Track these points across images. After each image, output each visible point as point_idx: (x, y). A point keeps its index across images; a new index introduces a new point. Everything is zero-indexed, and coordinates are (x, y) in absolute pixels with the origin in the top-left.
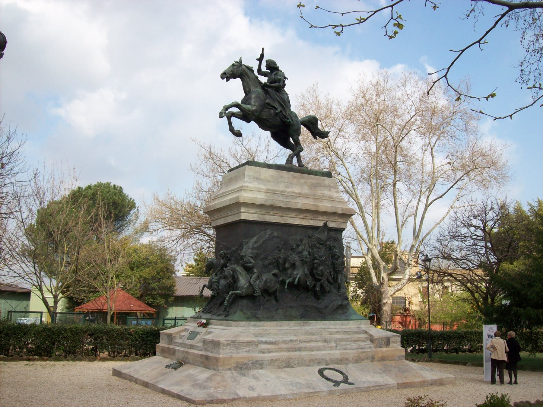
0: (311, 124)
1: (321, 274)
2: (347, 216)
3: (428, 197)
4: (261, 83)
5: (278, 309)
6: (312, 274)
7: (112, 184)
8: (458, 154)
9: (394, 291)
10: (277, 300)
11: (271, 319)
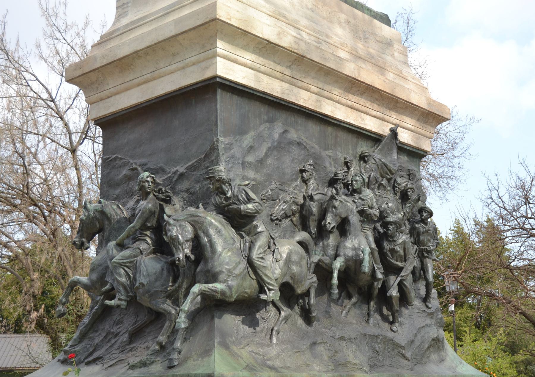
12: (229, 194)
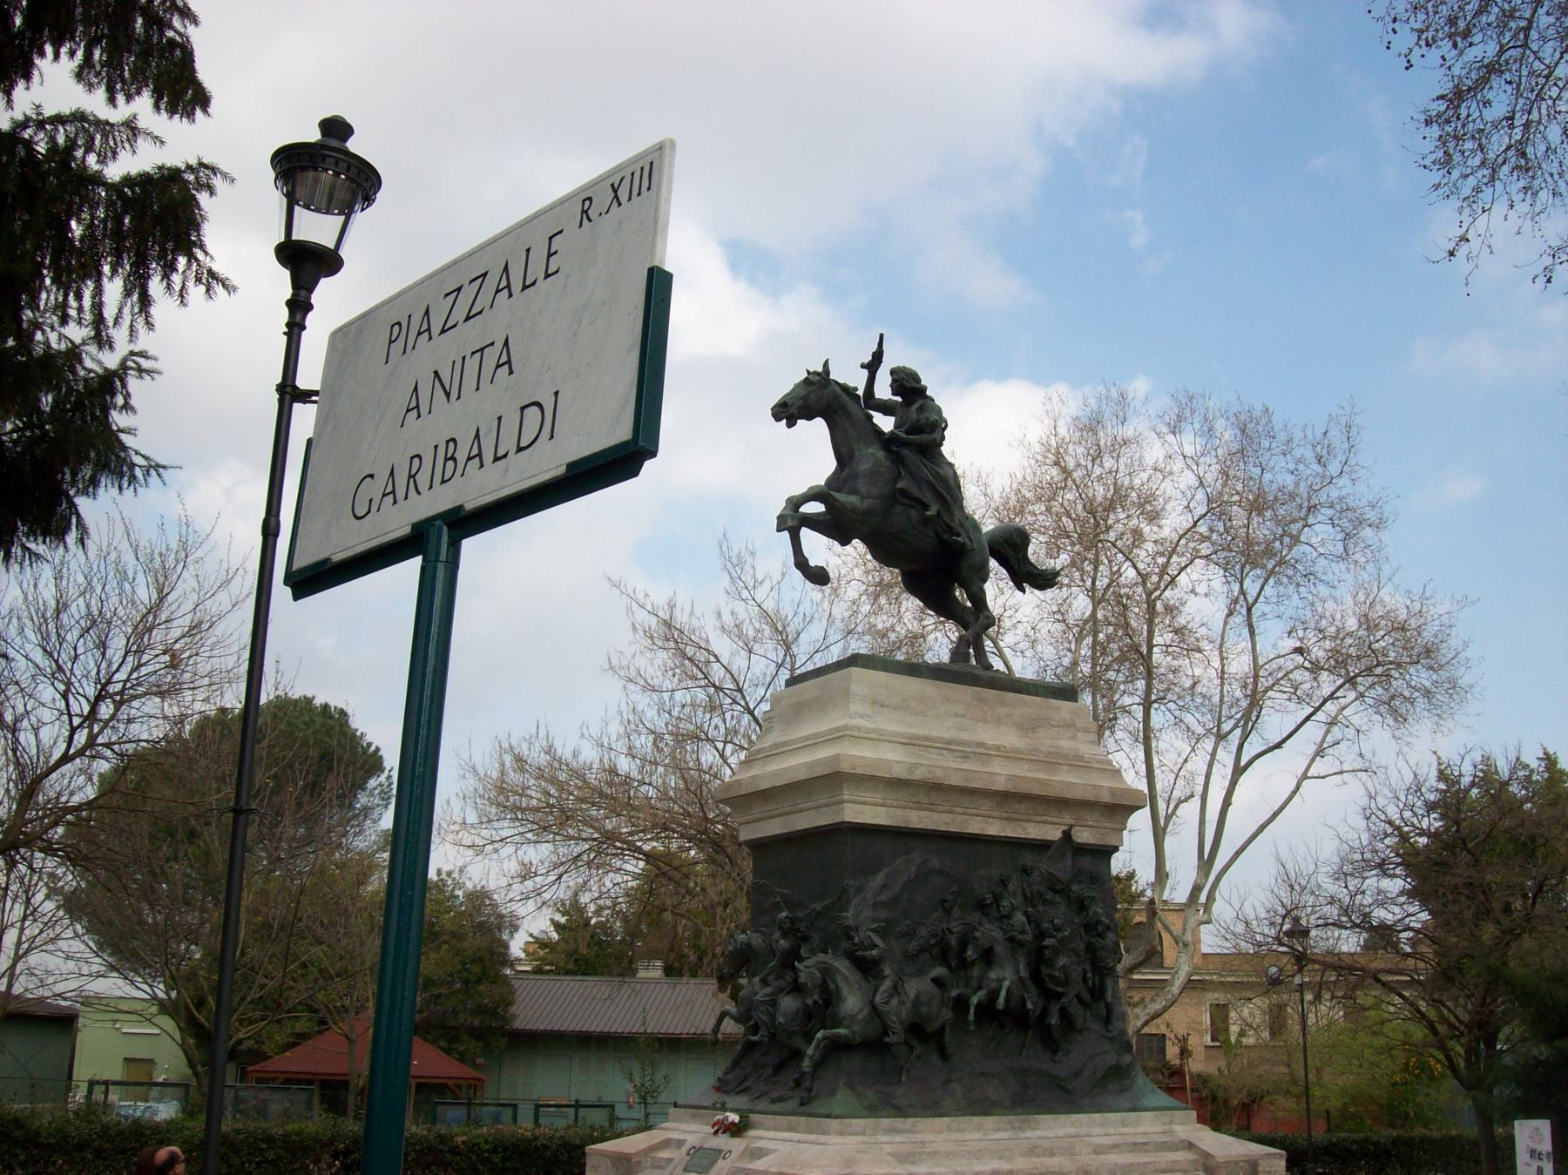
0: (1010, 549)
1: (1062, 978)
2: (1119, 809)
3: (1241, 747)
4: (877, 431)
5: (947, 1082)
6: (1036, 977)
7: (318, 702)
8: (1324, 623)
9: (1143, 1019)
10: (944, 1056)
11: (933, 1109)
12: (856, 940)
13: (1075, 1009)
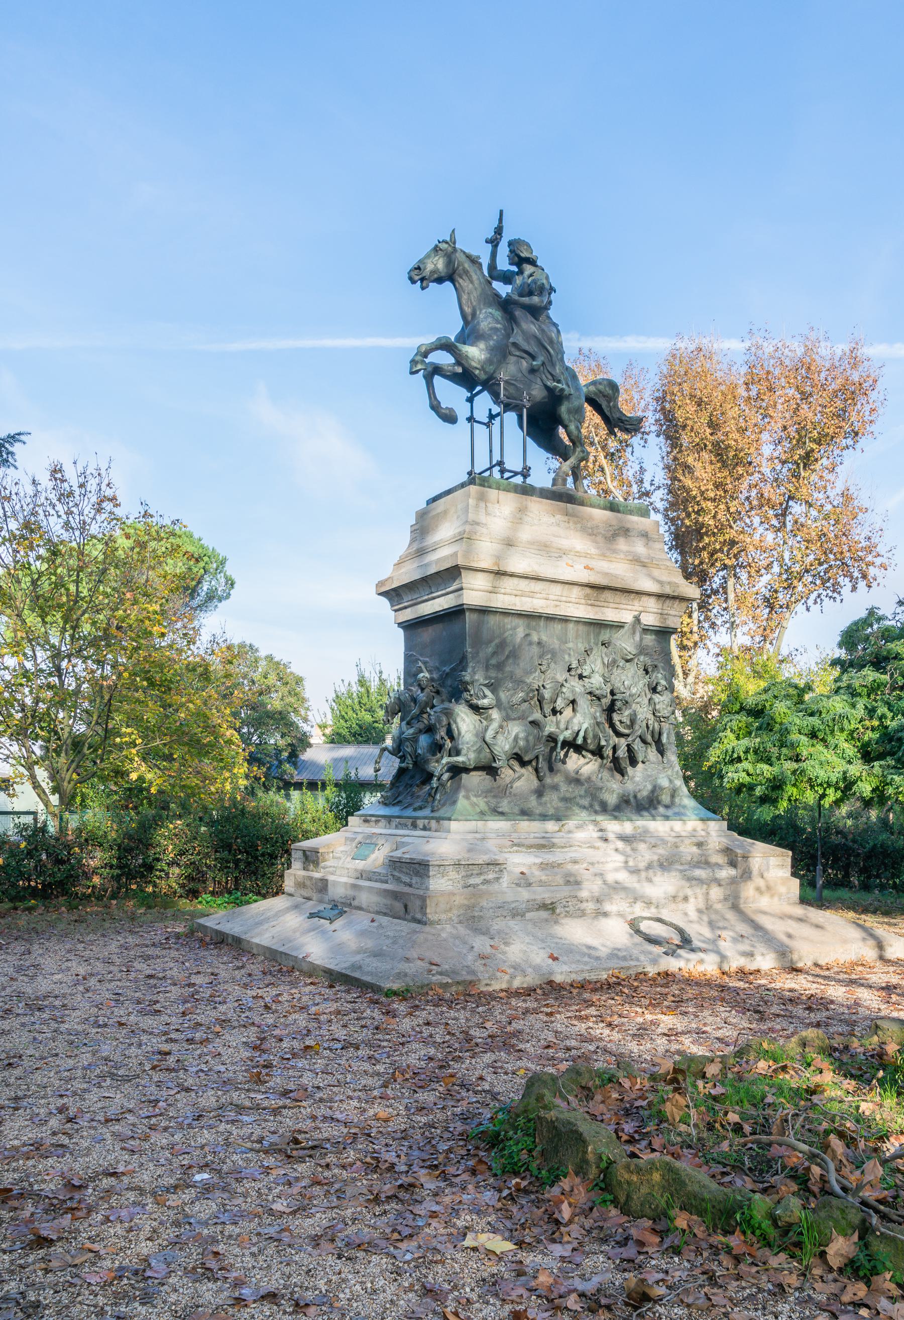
4: (497, 295)
7: (262, 653)
13: (638, 746)
